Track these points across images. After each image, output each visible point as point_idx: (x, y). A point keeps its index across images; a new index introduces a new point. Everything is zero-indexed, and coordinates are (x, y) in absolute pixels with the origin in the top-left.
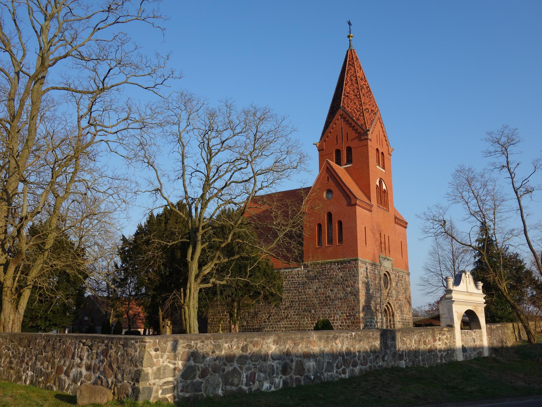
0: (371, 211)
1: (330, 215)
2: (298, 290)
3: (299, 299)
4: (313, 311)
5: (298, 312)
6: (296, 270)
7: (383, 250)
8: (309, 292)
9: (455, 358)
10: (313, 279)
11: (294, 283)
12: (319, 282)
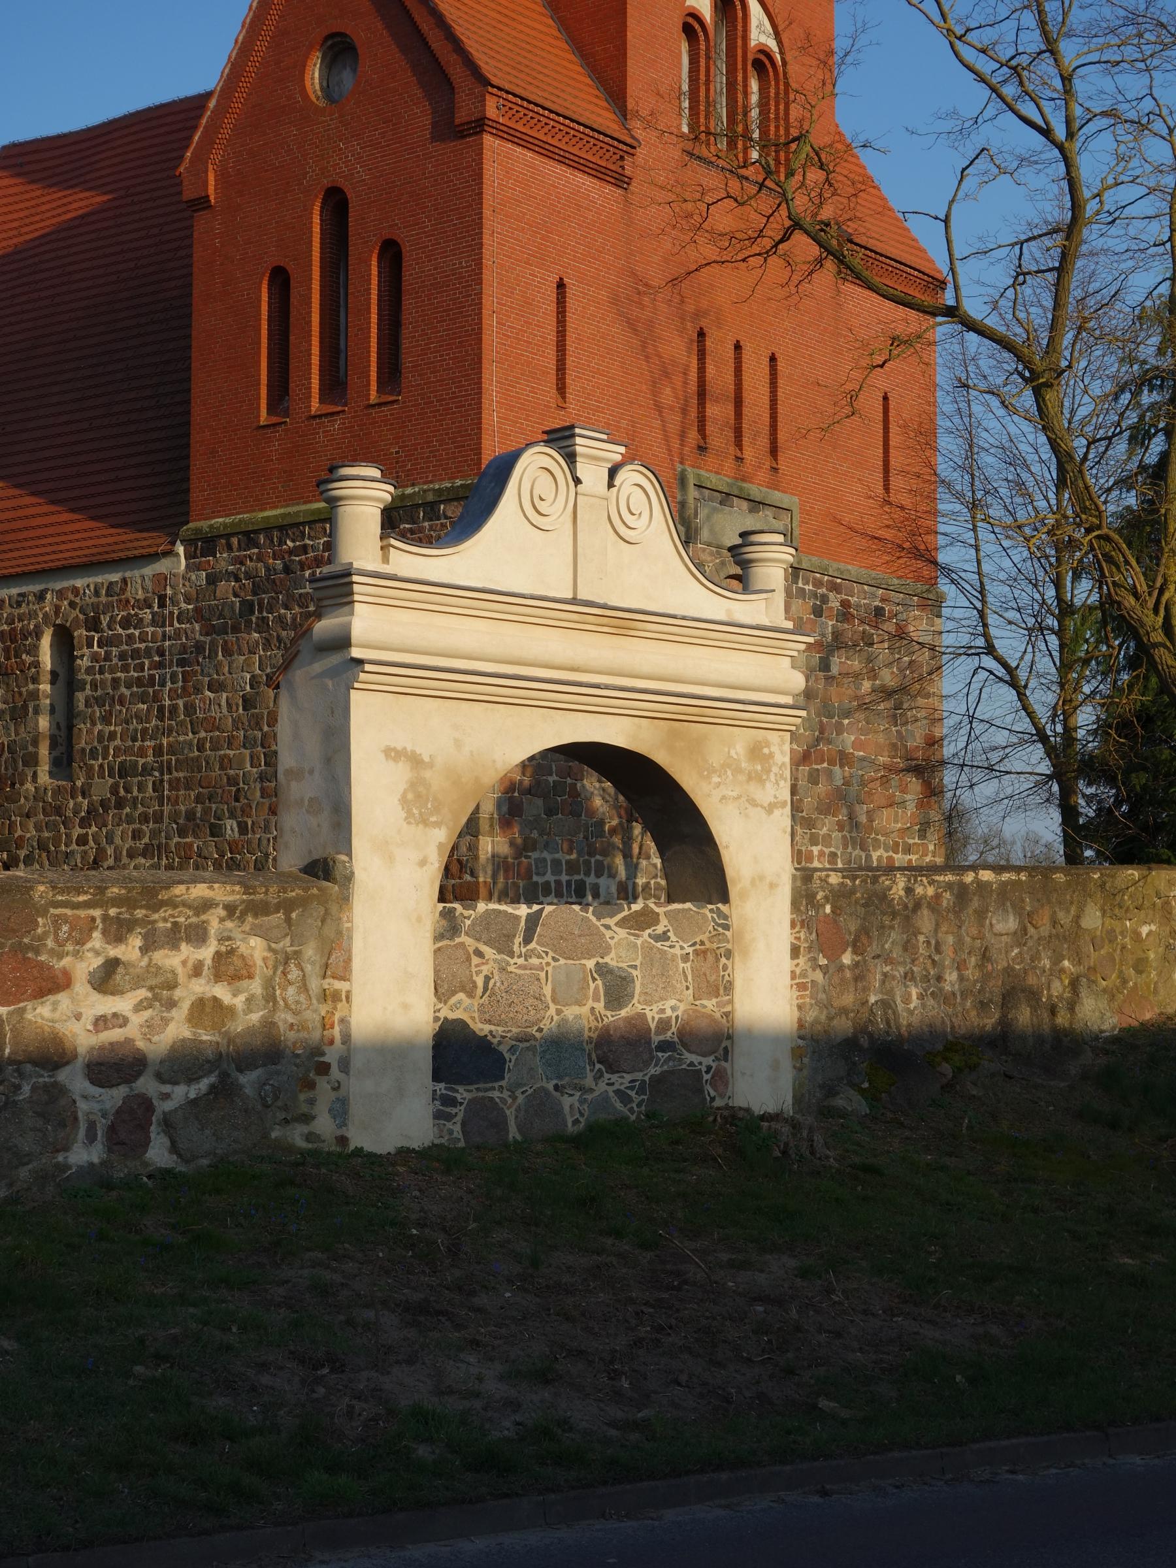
0: (621, 181)
1: (337, 203)
2: (156, 698)
3: (158, 750)
4: (230, 827)
5: (154, 834)
6: (149, 571)
7: (719, 438)
8: (214, 713)
9: (324, 1125)
10: (236, 629)
11: (136, 654)
12: (267, 645)
